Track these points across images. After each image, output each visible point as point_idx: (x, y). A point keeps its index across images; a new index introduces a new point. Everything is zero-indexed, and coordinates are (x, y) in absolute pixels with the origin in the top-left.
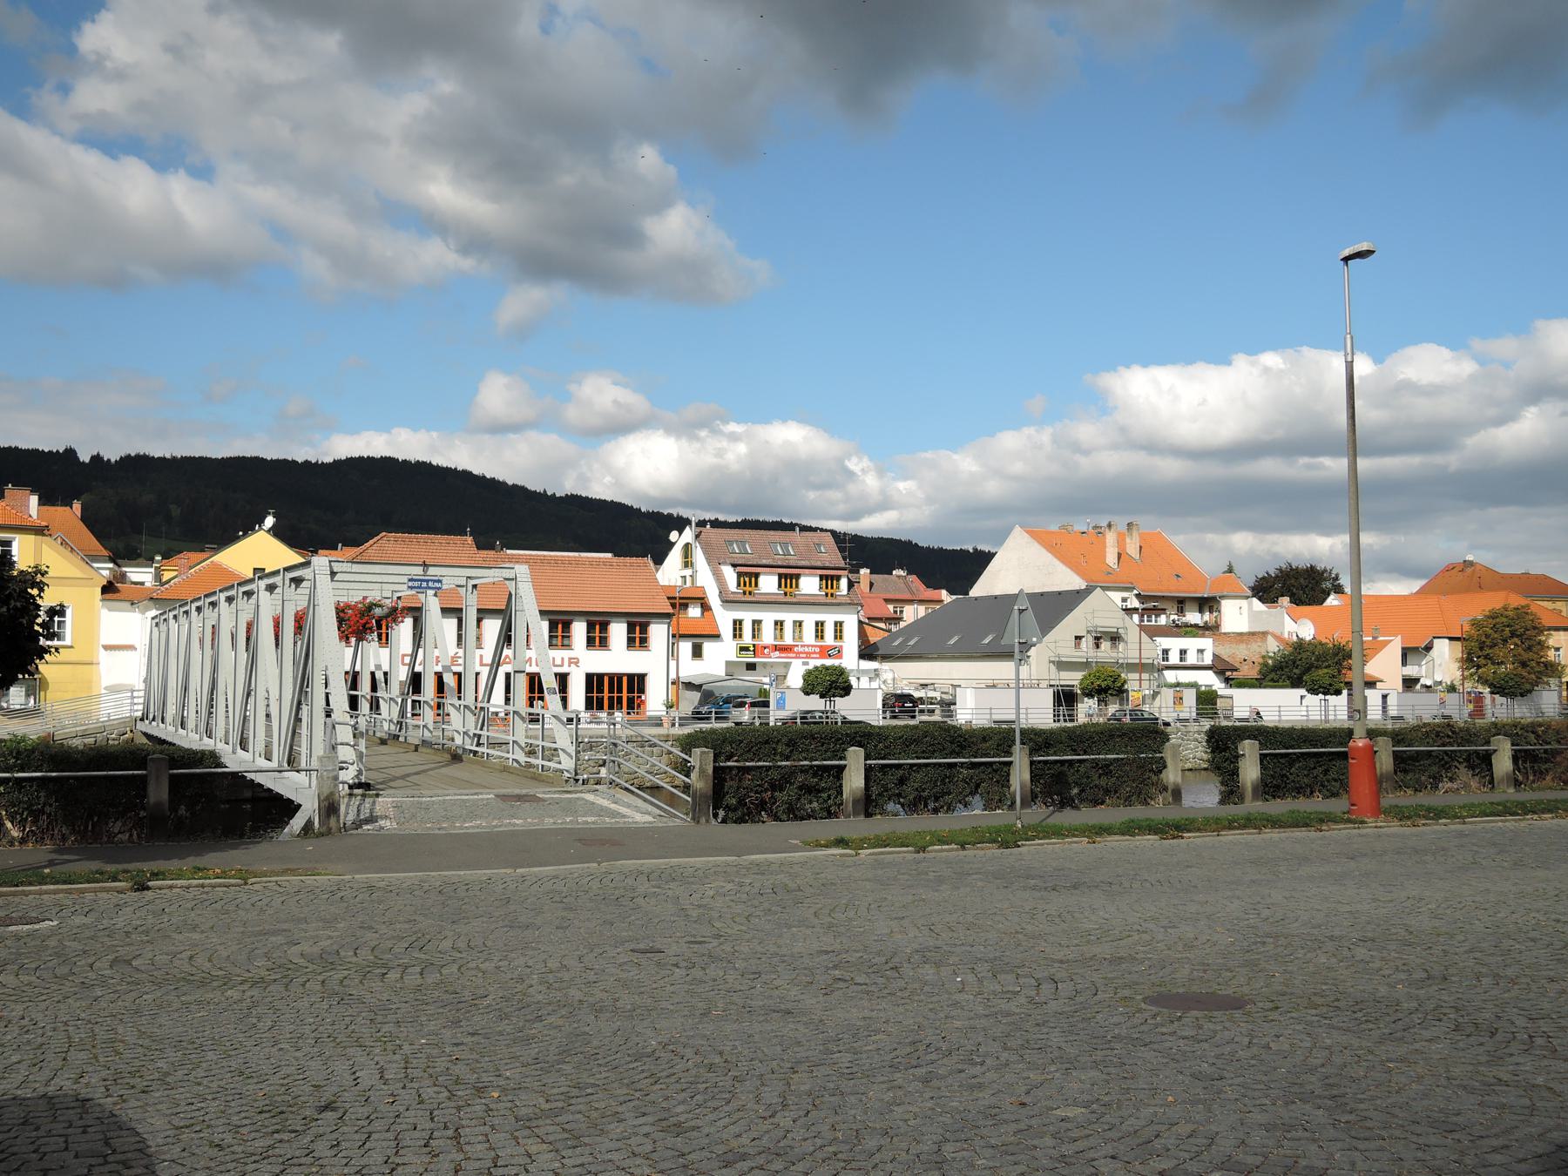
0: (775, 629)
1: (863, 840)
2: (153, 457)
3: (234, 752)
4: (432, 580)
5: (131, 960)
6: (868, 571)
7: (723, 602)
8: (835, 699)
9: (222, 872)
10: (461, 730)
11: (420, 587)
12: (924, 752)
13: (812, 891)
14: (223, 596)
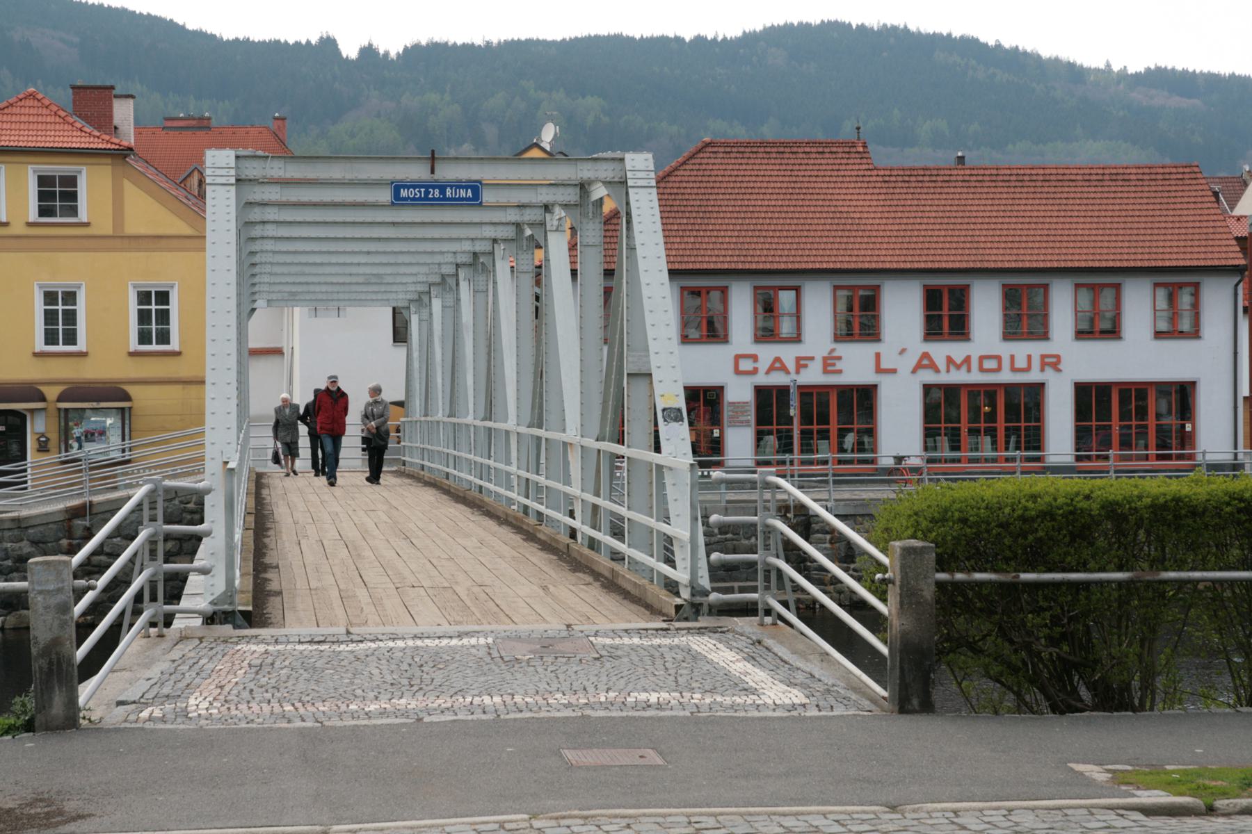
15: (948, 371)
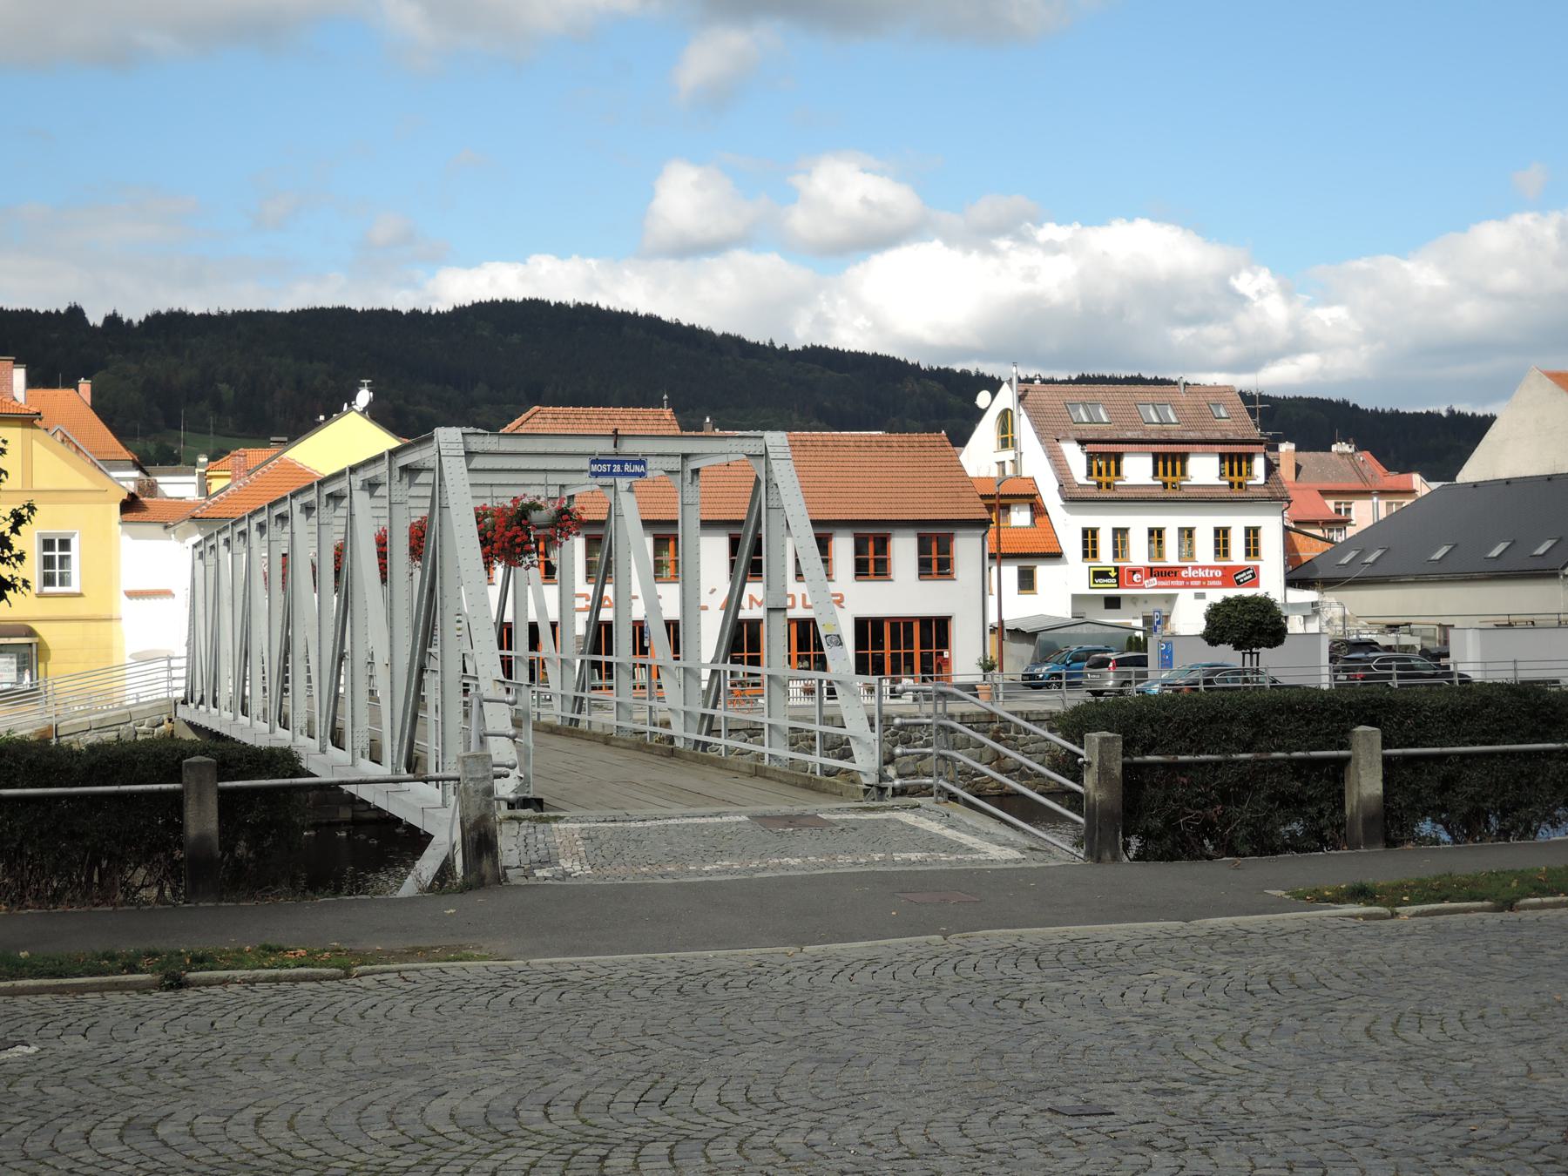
0: (1150, 542)
1: (1399, 888)
2: (193, 314)
3: (323, 751)
4: (629, 462)
5: (155, 1125)
6: (1292, 446)
7: (1065, 500)
8: (1259, 650)
9: (311, 954)
10: (680, 706)
11: (610, 473)
12: (1484, 732)
13: (1345, 986)
14: (297, 504)
15: (751, 608)
